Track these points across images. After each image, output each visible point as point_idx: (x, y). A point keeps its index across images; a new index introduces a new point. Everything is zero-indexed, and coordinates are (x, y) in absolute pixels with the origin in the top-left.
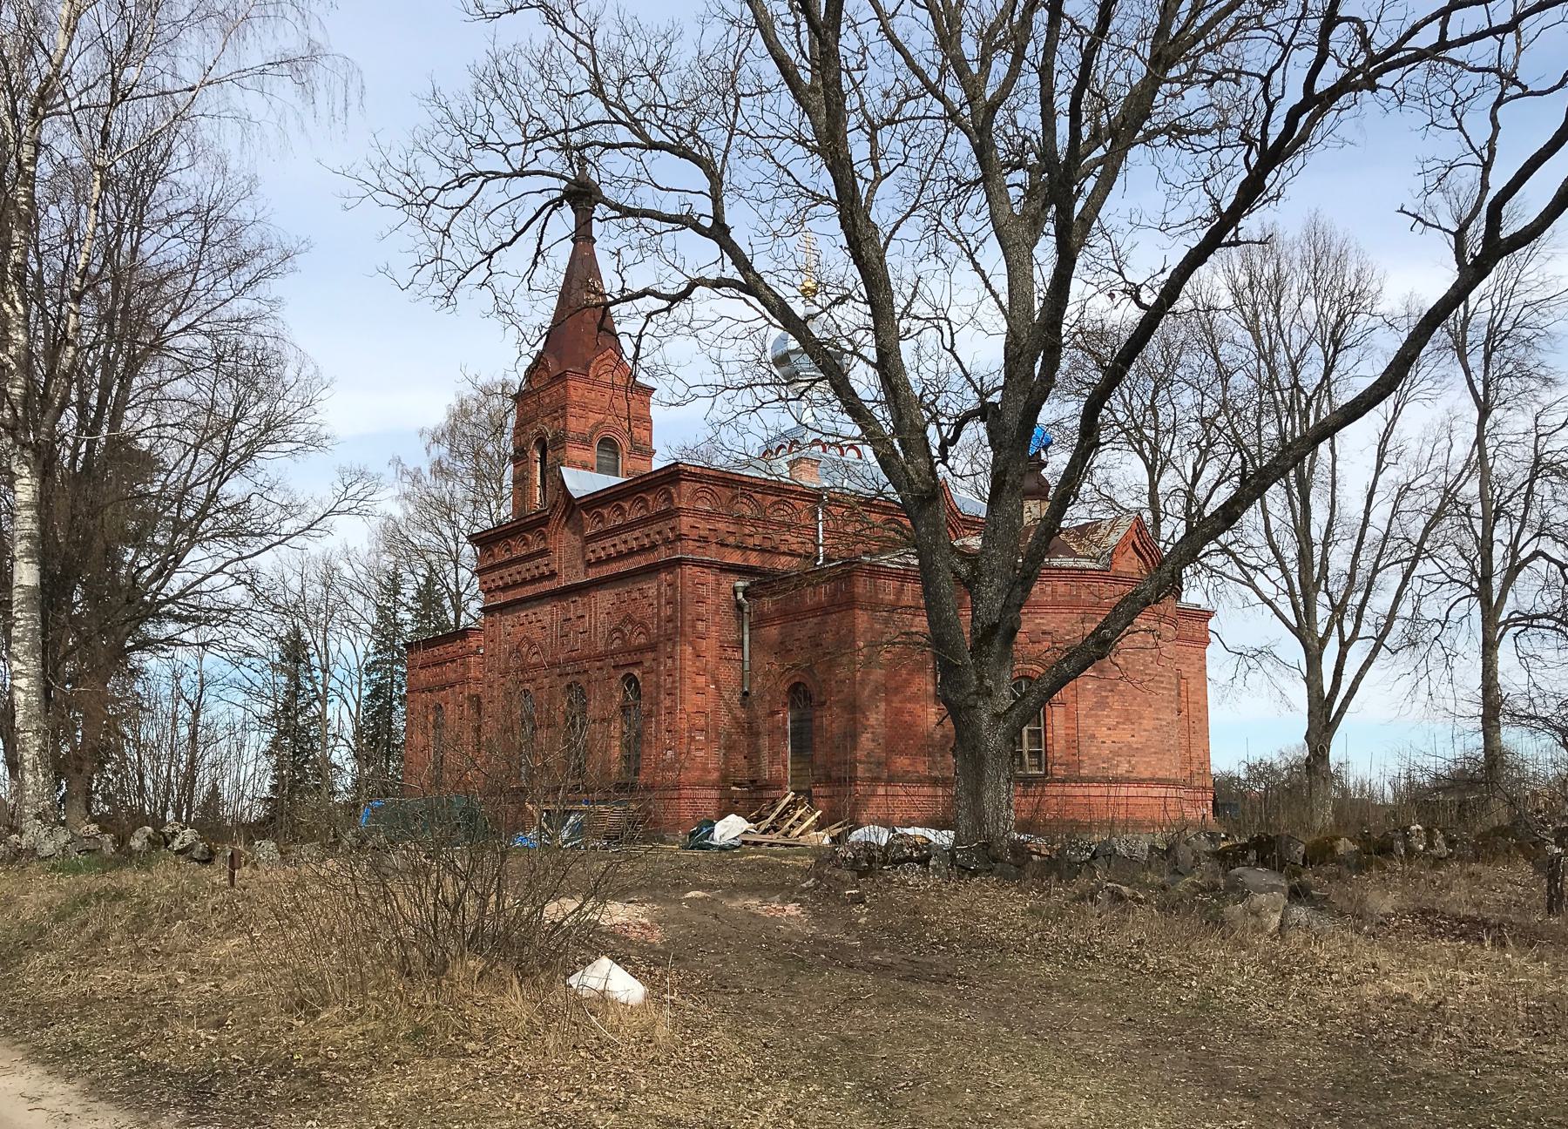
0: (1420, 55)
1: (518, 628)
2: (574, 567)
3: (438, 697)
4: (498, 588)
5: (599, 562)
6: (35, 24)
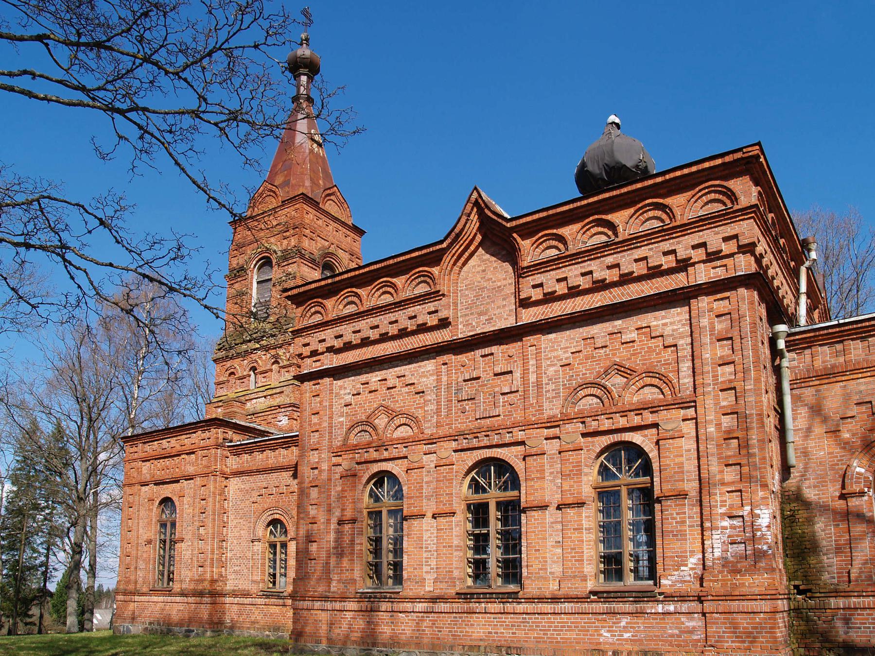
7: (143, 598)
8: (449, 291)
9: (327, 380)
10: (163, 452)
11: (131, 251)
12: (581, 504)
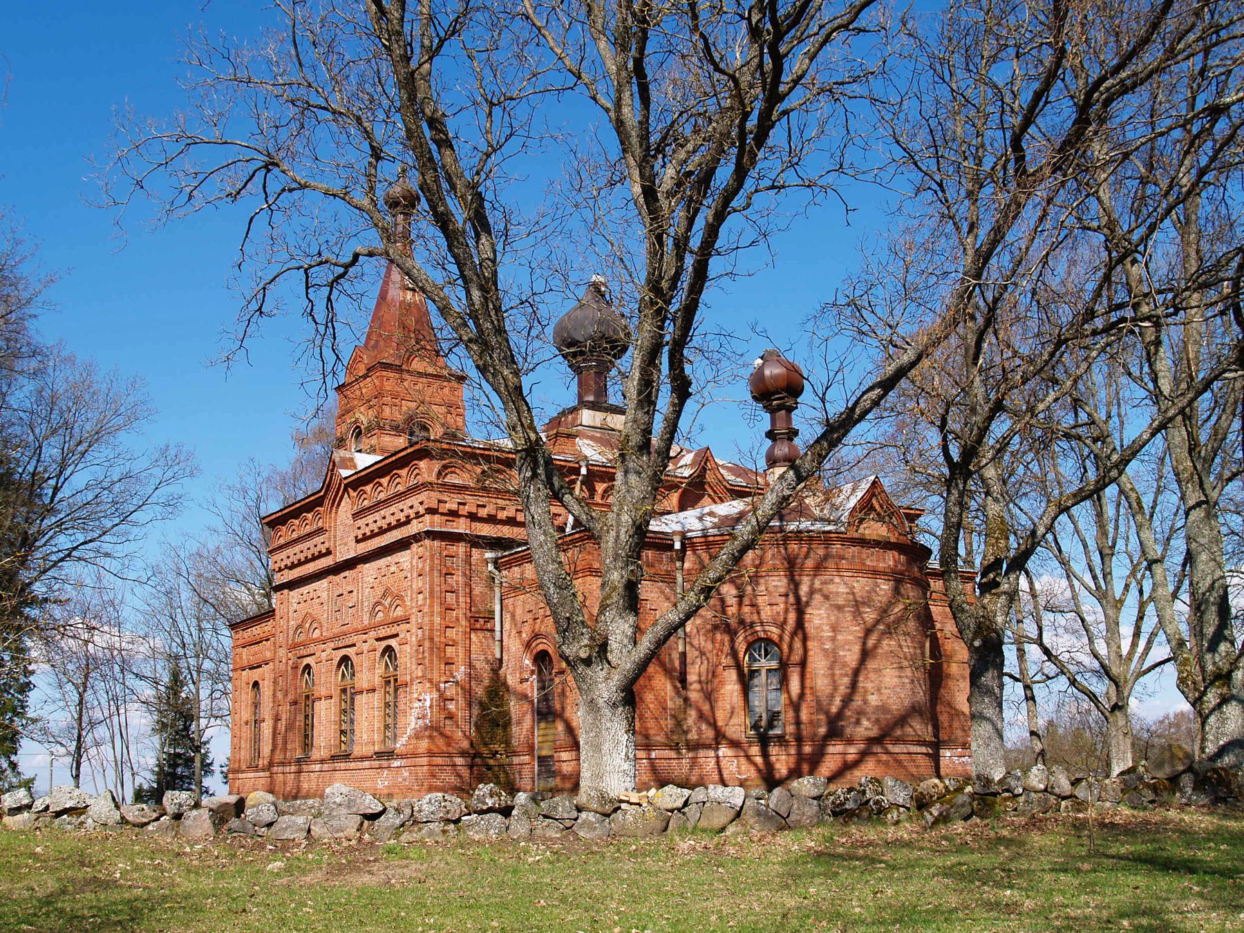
0: (967, 65)
1: (303, 604)
2: (346, 544)
3: (255, 675)
4: (286, 567)
5: (365, 538)
6: (633, 854)
7: (244, 775)
8: (330, 527)
9: (286, 591)
10: (254, 638)
11: (69, 555)
12: (374, 690)
